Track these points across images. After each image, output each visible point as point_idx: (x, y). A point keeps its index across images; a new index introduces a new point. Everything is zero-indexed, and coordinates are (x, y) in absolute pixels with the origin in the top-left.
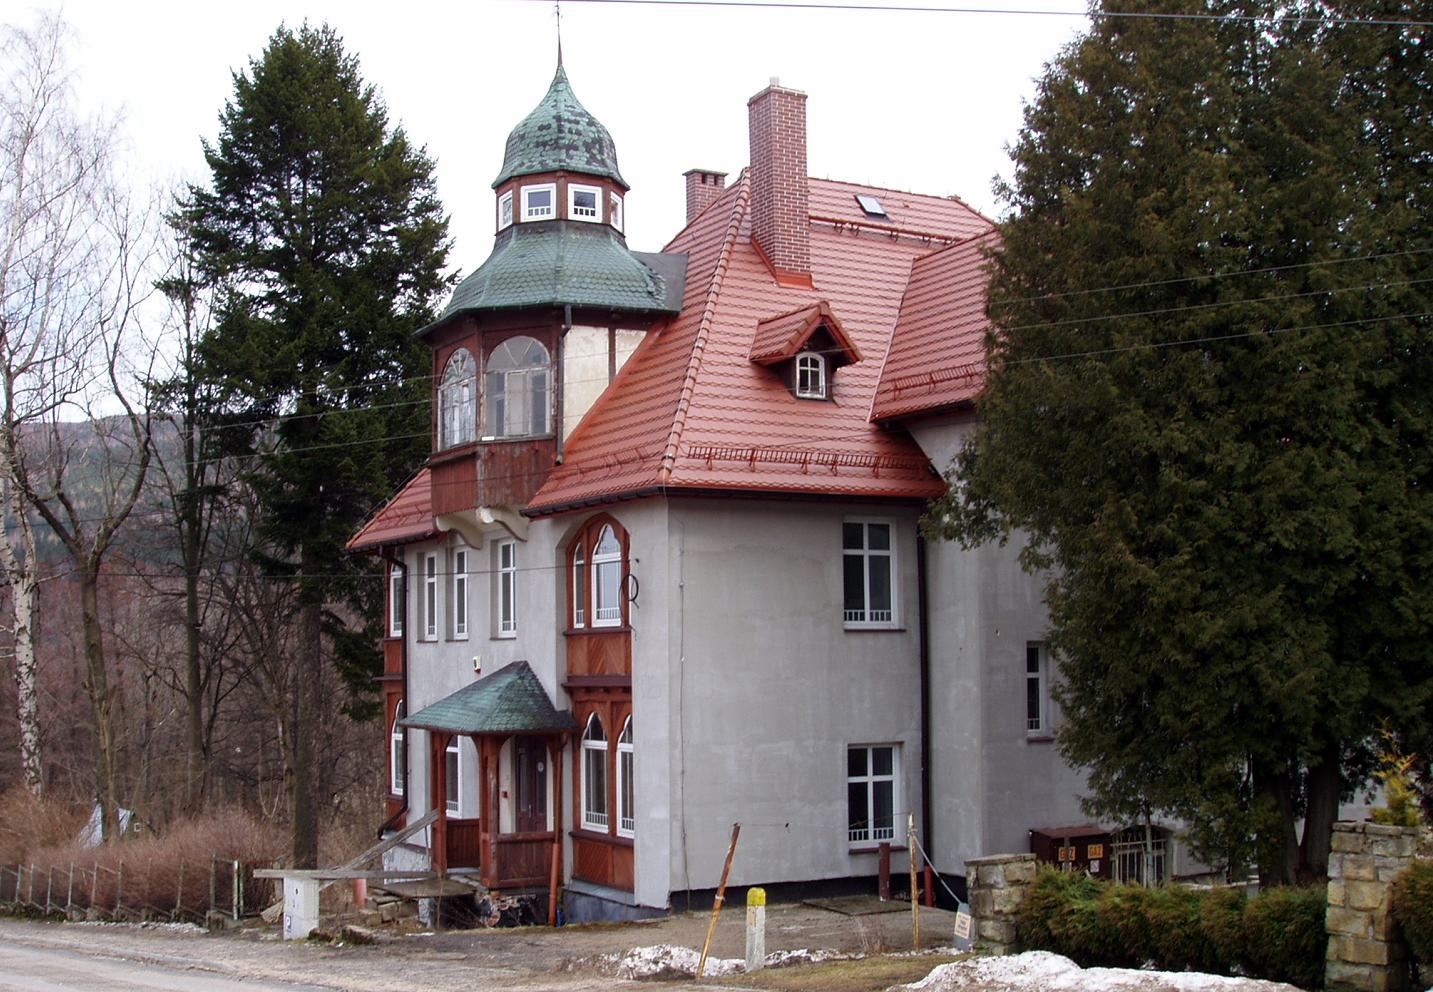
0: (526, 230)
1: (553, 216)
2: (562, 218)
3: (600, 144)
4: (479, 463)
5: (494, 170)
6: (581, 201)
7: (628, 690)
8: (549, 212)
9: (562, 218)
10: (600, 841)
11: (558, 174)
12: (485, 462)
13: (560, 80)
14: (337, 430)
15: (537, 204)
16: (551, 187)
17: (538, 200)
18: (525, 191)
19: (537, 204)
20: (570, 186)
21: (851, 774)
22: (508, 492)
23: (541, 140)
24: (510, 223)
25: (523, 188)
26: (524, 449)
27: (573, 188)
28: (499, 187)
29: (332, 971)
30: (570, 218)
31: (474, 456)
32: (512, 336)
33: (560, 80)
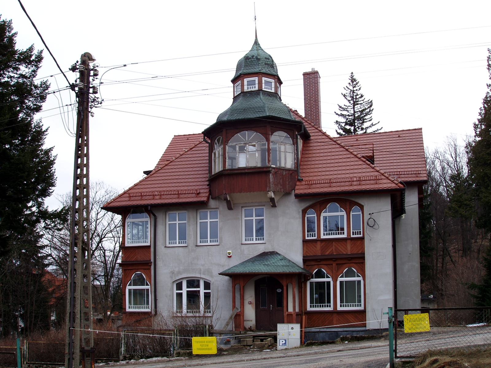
0: (265, 94)
1: (257, 88)
2: (260, 90)
3: (270, 63)
4: (271, 175)
5: (233, 75)
6: (268, 85)
7: (363, 258)
8: (255, 87)
9: (260, 90)
10: (243, 307)
11: (276, 77)
12: (273, 175)
13: (256, 43)
14: (428, 167)
15: (250, 84)
16: (256, 79)
17: (251, 83)
18: (246, 80)
19: (250, 84)
20: (263, 78)
21: (210, 293)
22: (281, 187)
23: (267, 62)
24: (240, 92)
25: (245, 79)
26: (287, 172)
27: (264, 79)
28: (234, 81)
29: (359, 344)
30: (263, 89)
31: (269, 172)
32: (279, 131)
33: (256, 43)
